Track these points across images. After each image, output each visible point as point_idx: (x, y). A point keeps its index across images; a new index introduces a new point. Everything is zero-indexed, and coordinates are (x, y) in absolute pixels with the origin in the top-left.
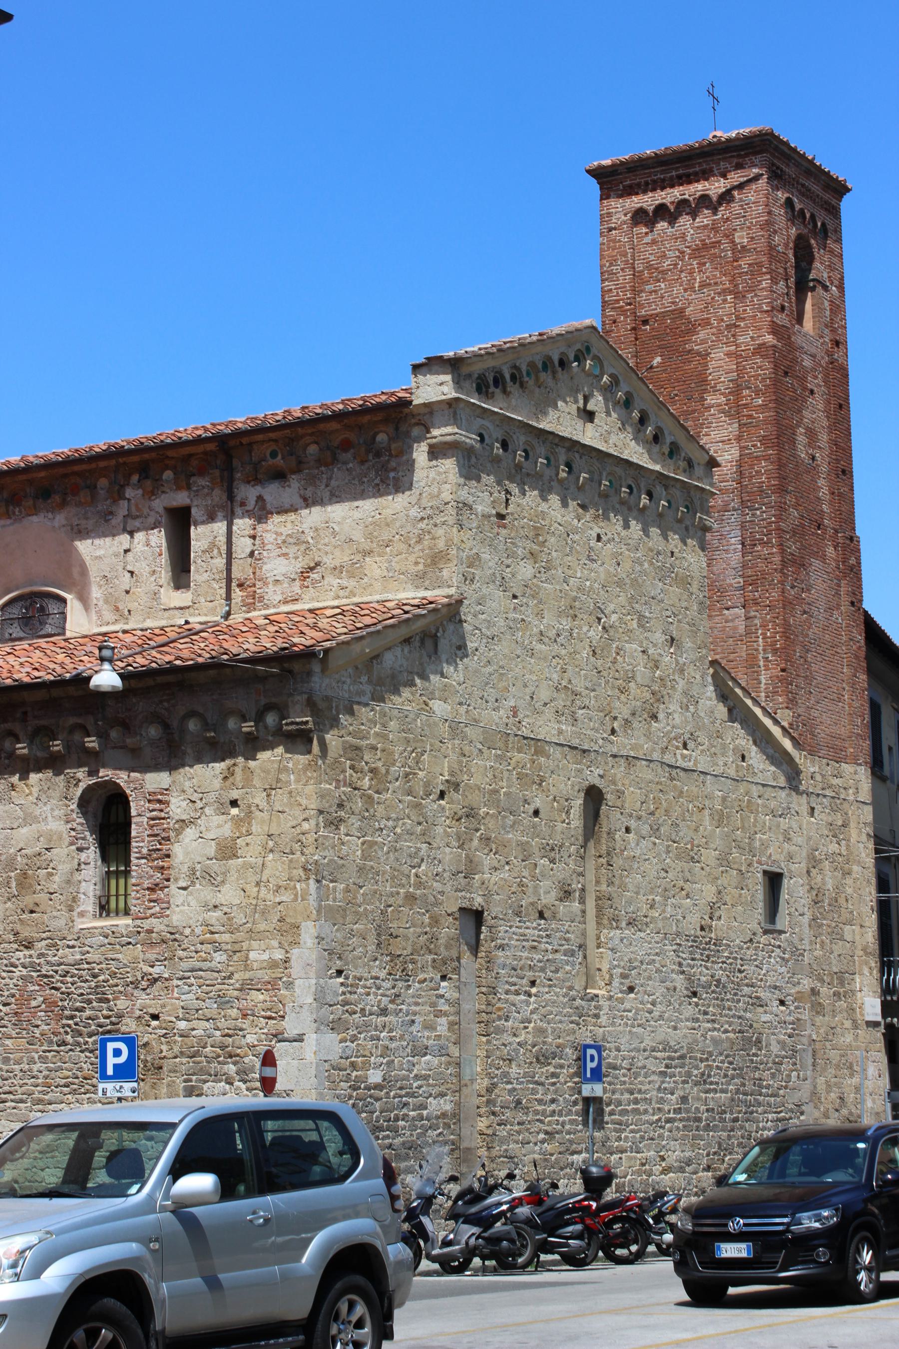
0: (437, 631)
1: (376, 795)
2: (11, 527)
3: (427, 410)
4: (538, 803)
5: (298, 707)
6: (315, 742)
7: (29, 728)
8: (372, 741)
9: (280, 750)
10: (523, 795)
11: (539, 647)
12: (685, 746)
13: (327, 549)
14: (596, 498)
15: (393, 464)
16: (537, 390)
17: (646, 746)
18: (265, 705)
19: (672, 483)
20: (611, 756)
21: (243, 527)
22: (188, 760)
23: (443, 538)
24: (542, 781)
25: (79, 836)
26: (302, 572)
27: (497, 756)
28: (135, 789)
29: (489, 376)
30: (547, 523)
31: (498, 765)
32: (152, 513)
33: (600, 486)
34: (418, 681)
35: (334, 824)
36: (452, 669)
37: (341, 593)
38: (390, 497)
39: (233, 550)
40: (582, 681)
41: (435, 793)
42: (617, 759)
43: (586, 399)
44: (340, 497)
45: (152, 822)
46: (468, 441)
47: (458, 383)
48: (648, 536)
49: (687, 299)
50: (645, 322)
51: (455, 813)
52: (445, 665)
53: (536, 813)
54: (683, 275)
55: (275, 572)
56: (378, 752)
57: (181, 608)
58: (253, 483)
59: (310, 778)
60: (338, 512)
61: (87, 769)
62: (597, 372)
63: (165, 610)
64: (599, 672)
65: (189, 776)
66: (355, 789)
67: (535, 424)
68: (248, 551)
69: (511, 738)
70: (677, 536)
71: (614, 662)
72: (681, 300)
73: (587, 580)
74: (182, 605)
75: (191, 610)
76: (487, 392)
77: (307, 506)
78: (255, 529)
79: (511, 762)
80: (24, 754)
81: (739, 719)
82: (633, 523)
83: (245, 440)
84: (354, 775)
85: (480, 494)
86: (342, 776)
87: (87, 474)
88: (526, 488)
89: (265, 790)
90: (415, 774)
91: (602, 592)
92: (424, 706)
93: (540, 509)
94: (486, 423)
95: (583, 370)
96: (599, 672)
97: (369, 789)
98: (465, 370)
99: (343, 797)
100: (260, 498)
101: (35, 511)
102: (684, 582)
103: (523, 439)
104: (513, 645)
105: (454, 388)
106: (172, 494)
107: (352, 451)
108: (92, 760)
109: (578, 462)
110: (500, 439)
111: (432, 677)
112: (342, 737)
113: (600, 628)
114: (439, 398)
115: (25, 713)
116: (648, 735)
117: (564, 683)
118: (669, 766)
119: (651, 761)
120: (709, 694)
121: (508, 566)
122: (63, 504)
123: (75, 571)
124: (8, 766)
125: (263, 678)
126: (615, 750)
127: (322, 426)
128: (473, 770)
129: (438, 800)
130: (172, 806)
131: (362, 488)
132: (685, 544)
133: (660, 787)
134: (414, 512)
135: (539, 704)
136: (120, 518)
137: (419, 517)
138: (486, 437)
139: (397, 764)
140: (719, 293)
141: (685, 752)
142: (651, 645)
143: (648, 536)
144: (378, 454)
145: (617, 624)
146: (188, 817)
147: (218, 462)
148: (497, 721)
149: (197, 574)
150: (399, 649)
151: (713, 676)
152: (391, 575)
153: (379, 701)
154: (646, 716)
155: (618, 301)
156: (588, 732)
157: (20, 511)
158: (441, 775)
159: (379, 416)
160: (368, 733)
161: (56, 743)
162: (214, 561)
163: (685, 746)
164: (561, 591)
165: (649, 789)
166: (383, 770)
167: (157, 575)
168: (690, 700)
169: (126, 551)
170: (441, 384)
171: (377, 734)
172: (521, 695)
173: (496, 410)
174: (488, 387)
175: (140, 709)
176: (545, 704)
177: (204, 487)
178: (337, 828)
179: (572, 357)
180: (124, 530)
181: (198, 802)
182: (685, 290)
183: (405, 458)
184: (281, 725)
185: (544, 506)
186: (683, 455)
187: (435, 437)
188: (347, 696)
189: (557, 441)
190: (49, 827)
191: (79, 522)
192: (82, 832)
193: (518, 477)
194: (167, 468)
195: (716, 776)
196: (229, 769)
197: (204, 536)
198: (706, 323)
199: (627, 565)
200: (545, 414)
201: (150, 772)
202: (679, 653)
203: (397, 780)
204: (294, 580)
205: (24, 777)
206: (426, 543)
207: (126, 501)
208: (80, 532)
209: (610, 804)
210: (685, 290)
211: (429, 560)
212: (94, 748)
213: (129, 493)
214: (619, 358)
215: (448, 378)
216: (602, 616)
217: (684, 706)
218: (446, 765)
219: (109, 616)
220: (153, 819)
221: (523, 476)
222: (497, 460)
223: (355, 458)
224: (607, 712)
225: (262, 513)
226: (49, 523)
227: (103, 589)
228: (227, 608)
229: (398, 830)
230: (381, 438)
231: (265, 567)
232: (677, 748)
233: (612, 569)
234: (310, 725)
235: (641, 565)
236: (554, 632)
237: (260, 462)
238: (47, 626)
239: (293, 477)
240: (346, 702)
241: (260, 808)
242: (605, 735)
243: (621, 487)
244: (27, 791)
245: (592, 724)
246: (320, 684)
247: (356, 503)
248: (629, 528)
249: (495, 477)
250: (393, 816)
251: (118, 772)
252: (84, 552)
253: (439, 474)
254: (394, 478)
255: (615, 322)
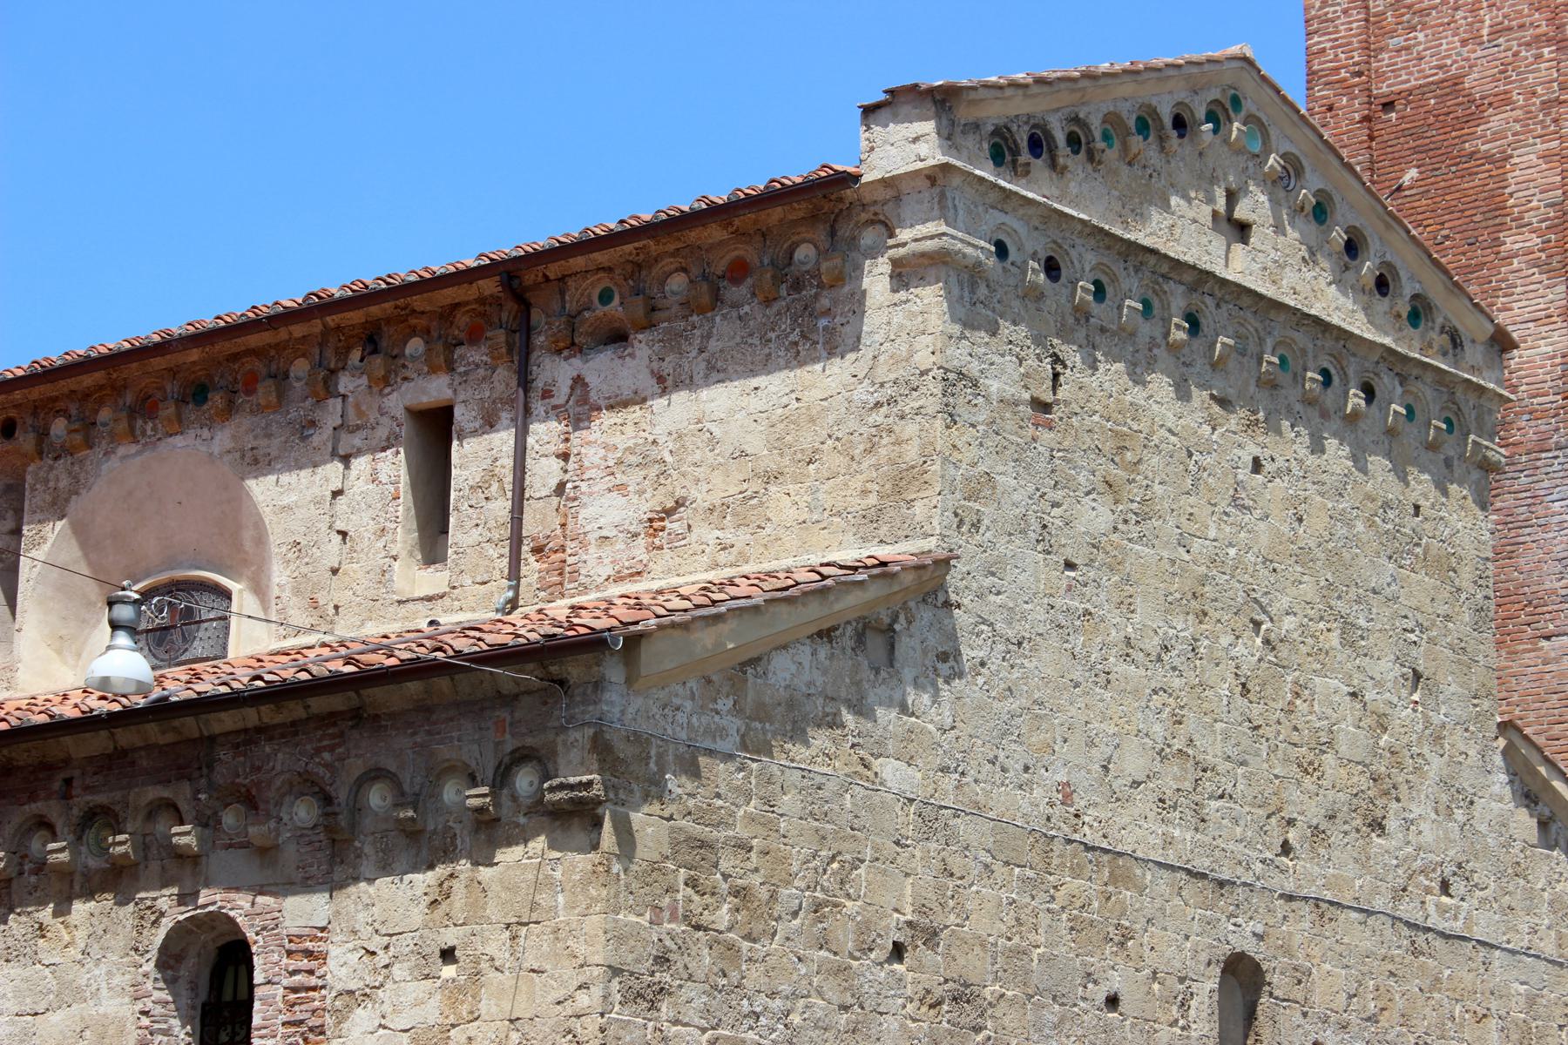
0: (895, 619)
1: (746, 945)
2: (138, 459)
3: (889, 193)
4: (1115, 982)
5: (575, 755)
6: (607, 825)
7: (75, 811)
8: (741, 831)
9: (539, 843)
10: (1084, 964)
11: (1120, 668)
12: (1445, 887)
13: (700, 472)
14: (1252, 388)
15: (825, 302)
16: (1125, 169)
17: (1358, 883)
18: (513, 752)
19: (1415, 372)
20: (1281, 896)
21: (546, 439)
22: (366, 868)
23: (916, 442)
24: (1126, 938)
25: (156, 1026)
26: (651, 520)
27: (1024, 880)
28: (264, 928)
29: (1022, 133)
30: (1143, 426)
31: (1028, 900)
32: (385, 420)
33: (1260, 364)
34: (848, 718)
35: (649, 997)
36: (926, 698)
37: (722, 557)
38: (818, 367)
39: (527, 482)
40: (1219, 745)
41: (882, 948)
42: (1295, 905)
43: (1232, 197)
44: (724, 370)
45: (292, 996)
46: (969, 250)
47: (948, 136)
48: (1364, 471)
49: (1467, 59)
50: (1388, 106)
51: (928, 992)
52: (909, 689)
53: (1113, 1001)
54: (1460, 14)
55: (602, 522)
56: (753, 855)
57: (429, 599)
58: (566, 353)
59: (595, 900)
60: (719, 399)
61: (175, 890)
62: (1256, 147)
63: (400, 602)
64: (1257, 728)
65: (366, 900)
66: (698, 928)
67: (1118, 232)
68: (553, 483)
69: (1057, 846)
70: (1426, 476)
71: (1289, 710)
72: (1455, 62)
73: (1231, 545)
74: (431, 593)
75: (447, 601)
76: (1014, 162)
77: (664, 392)
78: (567, 440)
79: (1057, 894)
80: (62, 863)
81: (1562, 842)
82: (1331, 444)
83: (553, 270)
84: (696, 898)
85: (996, 359)
86: (667, 900)
87: (273, 353)
88: (1099, 355)
89: (508, 926)
90: (836, 905)
91: (1264, 572)
92: (860, 768)
93: (1128, 398)
94: (1012, 221)
95: (1226, 141)
96: (1257, 728)
97: (730, 929)
98: (964, 114)
99: (668, 943)
100: (578, 381)
101: (179, 426)
102: (1445, 567)
103: (1091, 259)
104: (1066, 659)
105: (941, 147)
106: (420, 382)
107: (749, 281)
108: (186, 870)
109: (1211, 317)
110: (1043, 255)
111: (880, 711)
112: (670, 818)
113: (1259, 641)
114: (910, 168)
115: (68, 782)
116: (1363, 862)
117: (1177, 744)
118: (1408, 924)
119: (1369, 913)
120: (1496, 789)
121: (1055, 505)
122: (230, 410)
123: (247, 536)
124: (36, 888)
125: (508, 700)
126: (1290, 887)
127: (693, 235)
128: (969, 905)
129: (889, 961)
130: (332, 963)
131: (767, 351)
132: (1445, 493)
133: (1391, 967)
134: (862, 393)
135: (1120, 781)
136: (327, 432)
137: (872, 401)
138: (1012, 249)
139: (796, 883)
140: (1528, 44)
141: (1444, 899)
142: (1370, 683)
143: (1364, 471)
144: (797, 286)
145: (1295, 635)
146: (361, 985)
147: (504, 316)
148: (1026, 808)
149: (461, 533)
150: (808, 650)
151: (1505, 753)
152: (815, 517)
153: (758, 752)
154: (1358, 822)
155: (1336, 70)
156: (1231, 846)
157: (154, 429)
158: (896, 910)
159: (801, 209)
160: (732, 814)
161: (120, 838)
162: (491, 505)
163: (1445, 887)
164: (1173, 562)
165: (1365, 969)
166: (763, 894)
167: (389, 537)
168: (1454, 799)
169: (337, 494)
170: (916, 140)
171: (752, 819)
172: (1082, 761)
173: (1030, 195)
174: (1015, 152)
175: (278, 768)
176: (1136, 784)
177: (478, 366)
178: (653, 1006)
179: (1201, 113)
180: (334, 454)
181: (381, 953)
182: (1464, 42)
183: (846, 289)
184: (543, 791)
185: (1137, 394)
186: (1440, 320)
187: (904, 245)
188: (683, 735)
189: (1165, 268)
190: (102, 1010)
191: (255, 444)
192: (165, 1018)
193: (1081, 334)
194: (413, 332)
195: (1513, 952)
196: (441, 885)
197: (476, 457)
198: (1505, 100)
199: (1317, 523)
200: (1143, 217)
201: (295, 893)
202: (1431, 702)
203: (795, 914)
204: (636, 535)
205: (62, 911)
206: (883, 451)
207: (340, 400)
208: (256, 461)
209: (1277, 993)
210: (1464, 42)
211: (888, 486)
212: (188, 846)
213: (345, 383)
214: (1300, 123)
215: (928, 127)
216: (1263, 617)
217: (1441, 808)
218: (909, 890)
219: (299, 617)
220: (295, 990)
221: (1089, 330)
222: (1034, 296)
223: (754, 295)
224: (1272, 809)
225: (580, 409)
226: (203, 449)
227: (292, 567)
228: (511, 594)
229: (796, 1019)
230: (805, 253)
231: (583, 513)
232: (1428, 891)
233: (1285, 528)
234: (597, 790)
235: (1351, 526)
236: (1156, 641)
237: (579, 313)
238: (196, 643)
239: (640, 337)
240: (682, 749)
241: (497, 964)
242: (1268, 855)
243: (1305, 370)
244: (67, 938)
245: (1239, 830)
246: (622, 706)
247: (755, 382)
248: (1323, 451)
249: (1030, 328)
250: (785, 988)
251: (232, 895)
252: (261, 498)
253: (912, 316)
254: (825, 328)
255: (1330, 109)
